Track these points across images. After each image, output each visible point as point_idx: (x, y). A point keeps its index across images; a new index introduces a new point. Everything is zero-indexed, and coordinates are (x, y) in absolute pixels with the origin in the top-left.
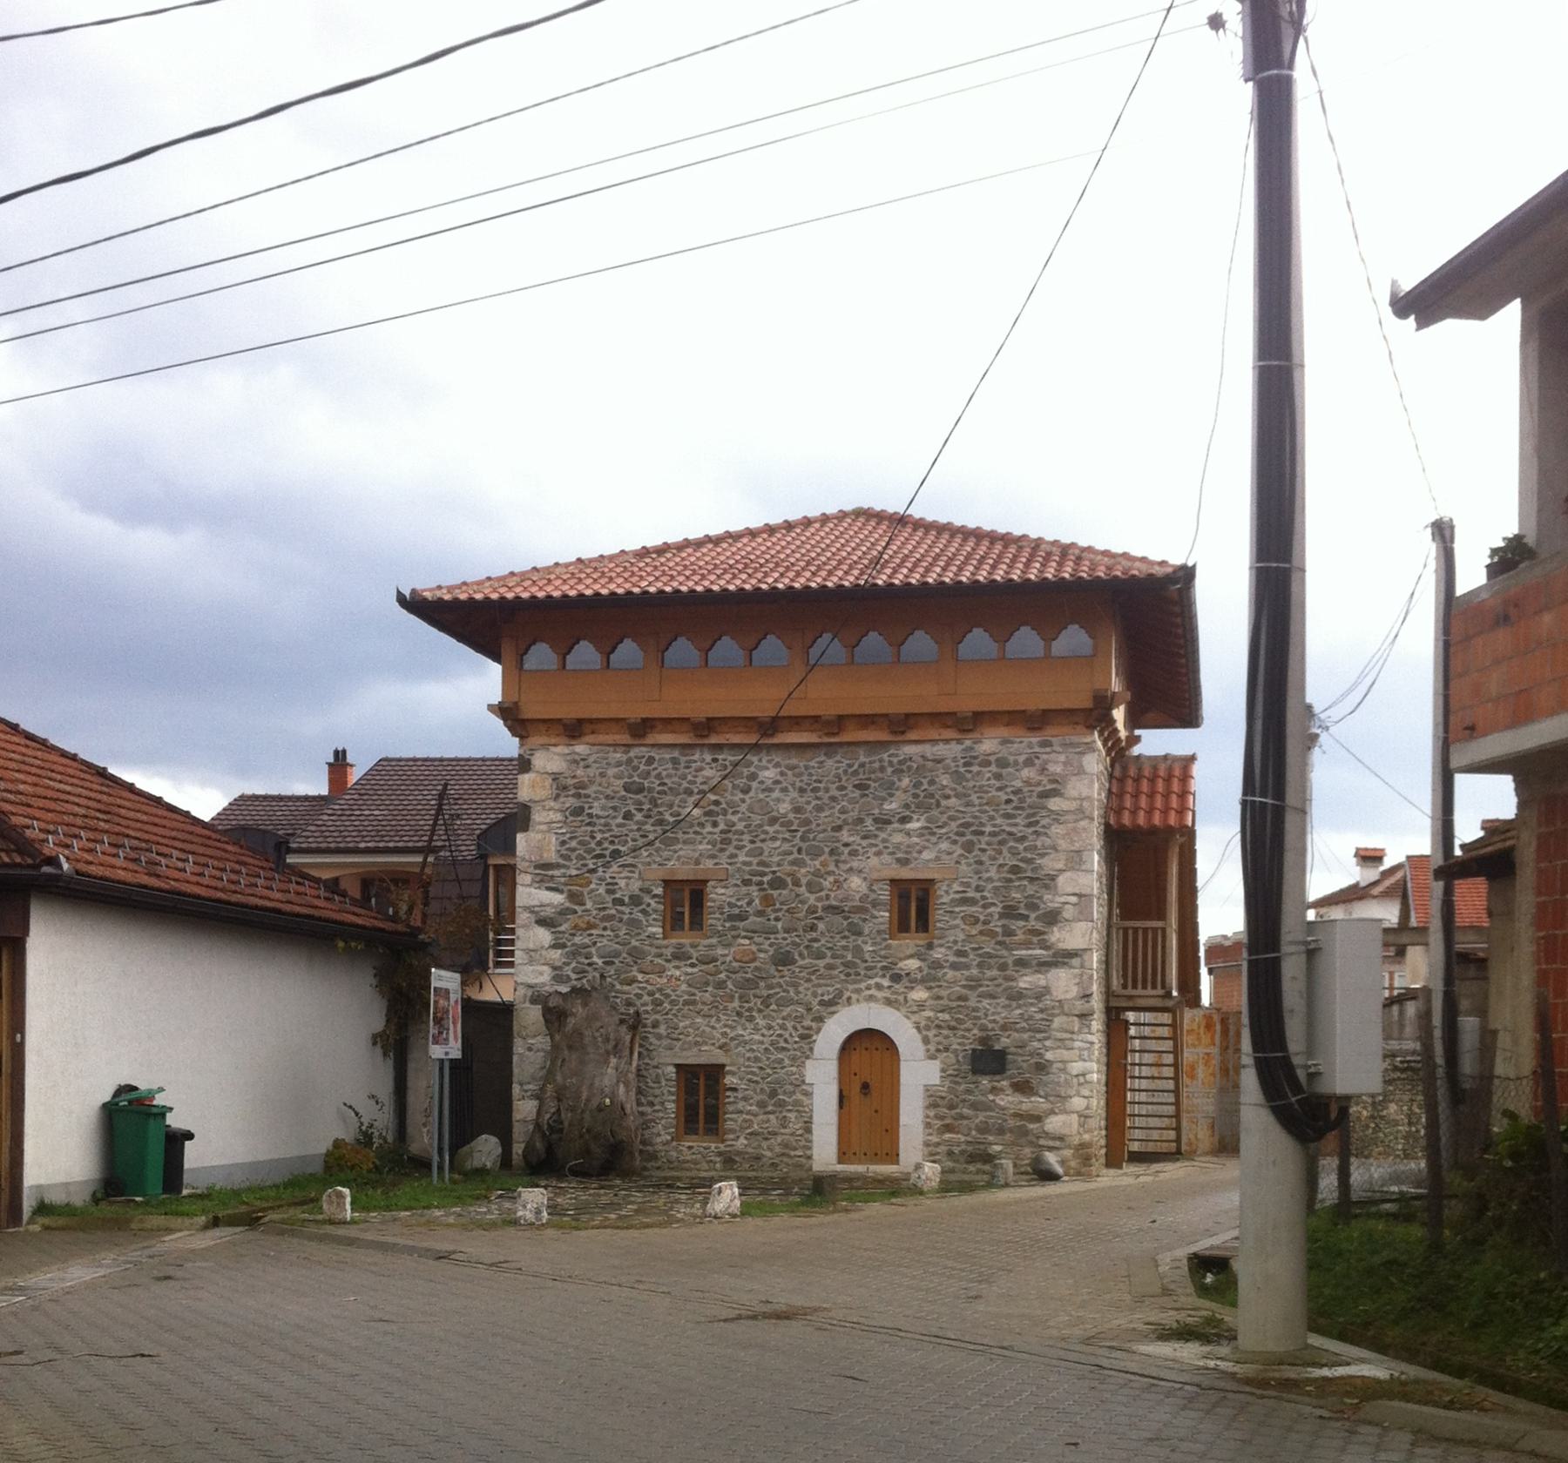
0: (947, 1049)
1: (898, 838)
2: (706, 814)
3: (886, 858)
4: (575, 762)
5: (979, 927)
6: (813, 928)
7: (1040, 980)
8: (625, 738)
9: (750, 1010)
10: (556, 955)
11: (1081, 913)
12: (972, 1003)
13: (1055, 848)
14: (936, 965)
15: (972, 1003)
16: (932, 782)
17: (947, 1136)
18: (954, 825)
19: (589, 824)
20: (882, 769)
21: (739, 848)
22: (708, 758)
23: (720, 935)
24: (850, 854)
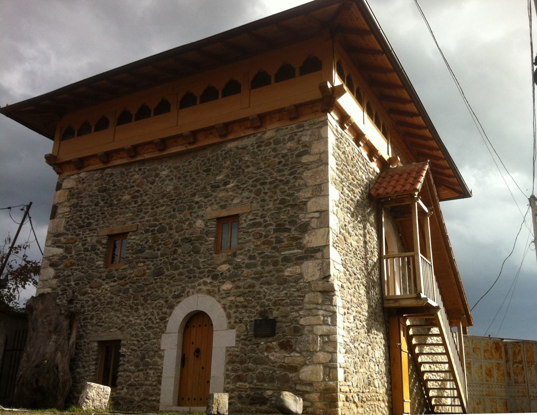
0: (241, 321)
1: (222, 194)
2: (133, 198)
3: (216, 207)
4: (80, 181)
5: (263, 239)
6: (175, 252)
7: (297, 269)
8: (101, 166)
9: (137, 305)
10: (54, 282)
11: (321, 223)
12: (257, 289)
13: (306, 185)
14: (238, 267)
15: (257, 289)
16: (241, 160)
17: (239, 384)
18: (251, 181)
19: (80, 211)
20: (217, 159)
21: (146, 213)
22: (137, 169)
23: (130, 262)
24: (199, 208)
